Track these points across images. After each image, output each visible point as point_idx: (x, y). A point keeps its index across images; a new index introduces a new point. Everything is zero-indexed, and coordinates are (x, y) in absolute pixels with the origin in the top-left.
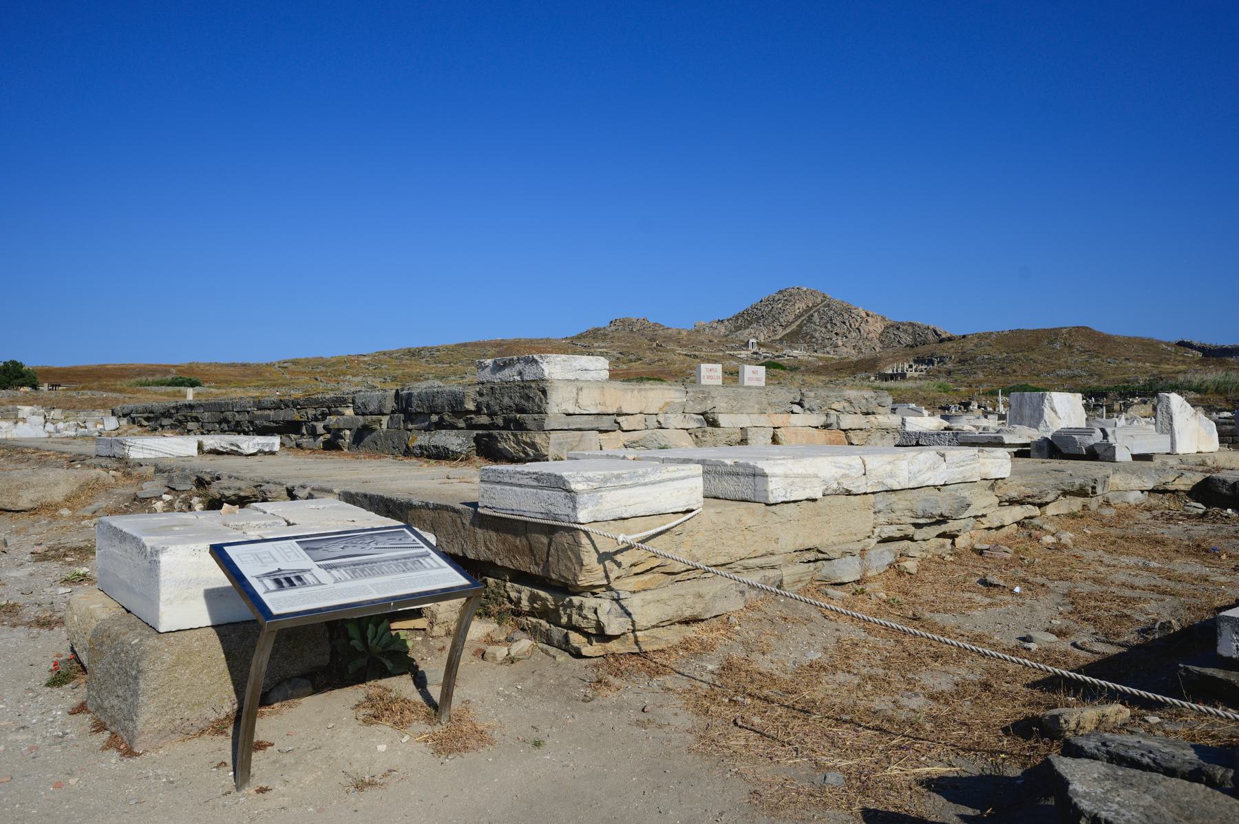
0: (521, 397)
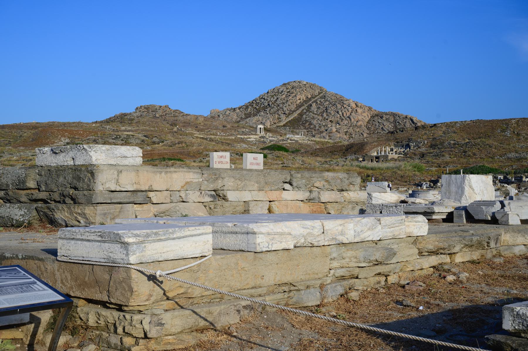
0: (73, 178)
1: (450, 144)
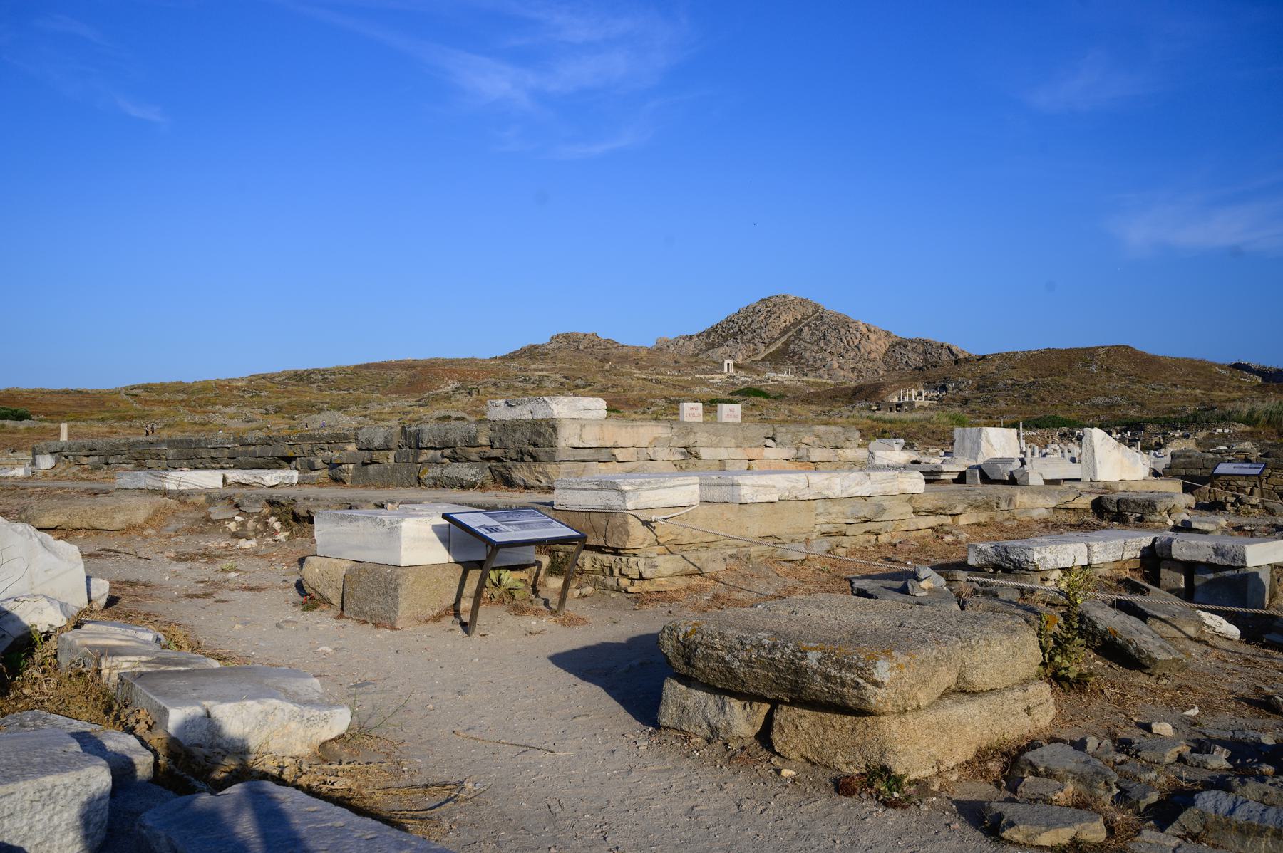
1: (1006, 384)
